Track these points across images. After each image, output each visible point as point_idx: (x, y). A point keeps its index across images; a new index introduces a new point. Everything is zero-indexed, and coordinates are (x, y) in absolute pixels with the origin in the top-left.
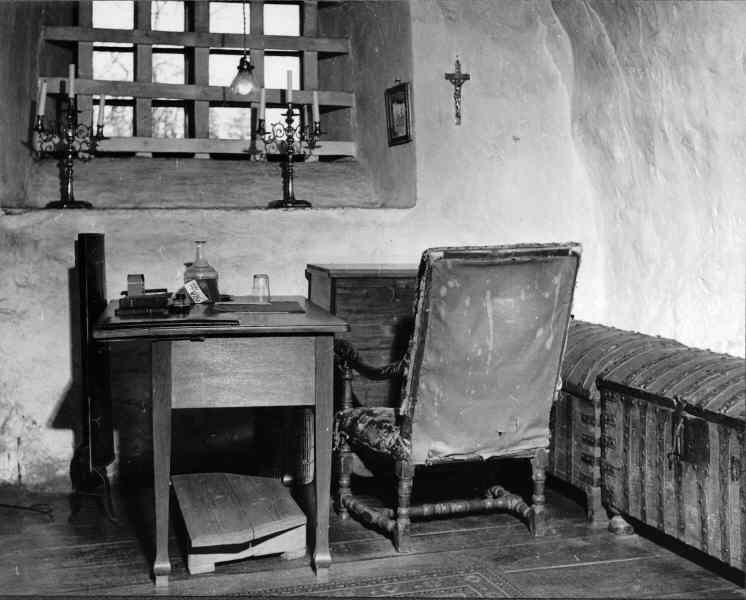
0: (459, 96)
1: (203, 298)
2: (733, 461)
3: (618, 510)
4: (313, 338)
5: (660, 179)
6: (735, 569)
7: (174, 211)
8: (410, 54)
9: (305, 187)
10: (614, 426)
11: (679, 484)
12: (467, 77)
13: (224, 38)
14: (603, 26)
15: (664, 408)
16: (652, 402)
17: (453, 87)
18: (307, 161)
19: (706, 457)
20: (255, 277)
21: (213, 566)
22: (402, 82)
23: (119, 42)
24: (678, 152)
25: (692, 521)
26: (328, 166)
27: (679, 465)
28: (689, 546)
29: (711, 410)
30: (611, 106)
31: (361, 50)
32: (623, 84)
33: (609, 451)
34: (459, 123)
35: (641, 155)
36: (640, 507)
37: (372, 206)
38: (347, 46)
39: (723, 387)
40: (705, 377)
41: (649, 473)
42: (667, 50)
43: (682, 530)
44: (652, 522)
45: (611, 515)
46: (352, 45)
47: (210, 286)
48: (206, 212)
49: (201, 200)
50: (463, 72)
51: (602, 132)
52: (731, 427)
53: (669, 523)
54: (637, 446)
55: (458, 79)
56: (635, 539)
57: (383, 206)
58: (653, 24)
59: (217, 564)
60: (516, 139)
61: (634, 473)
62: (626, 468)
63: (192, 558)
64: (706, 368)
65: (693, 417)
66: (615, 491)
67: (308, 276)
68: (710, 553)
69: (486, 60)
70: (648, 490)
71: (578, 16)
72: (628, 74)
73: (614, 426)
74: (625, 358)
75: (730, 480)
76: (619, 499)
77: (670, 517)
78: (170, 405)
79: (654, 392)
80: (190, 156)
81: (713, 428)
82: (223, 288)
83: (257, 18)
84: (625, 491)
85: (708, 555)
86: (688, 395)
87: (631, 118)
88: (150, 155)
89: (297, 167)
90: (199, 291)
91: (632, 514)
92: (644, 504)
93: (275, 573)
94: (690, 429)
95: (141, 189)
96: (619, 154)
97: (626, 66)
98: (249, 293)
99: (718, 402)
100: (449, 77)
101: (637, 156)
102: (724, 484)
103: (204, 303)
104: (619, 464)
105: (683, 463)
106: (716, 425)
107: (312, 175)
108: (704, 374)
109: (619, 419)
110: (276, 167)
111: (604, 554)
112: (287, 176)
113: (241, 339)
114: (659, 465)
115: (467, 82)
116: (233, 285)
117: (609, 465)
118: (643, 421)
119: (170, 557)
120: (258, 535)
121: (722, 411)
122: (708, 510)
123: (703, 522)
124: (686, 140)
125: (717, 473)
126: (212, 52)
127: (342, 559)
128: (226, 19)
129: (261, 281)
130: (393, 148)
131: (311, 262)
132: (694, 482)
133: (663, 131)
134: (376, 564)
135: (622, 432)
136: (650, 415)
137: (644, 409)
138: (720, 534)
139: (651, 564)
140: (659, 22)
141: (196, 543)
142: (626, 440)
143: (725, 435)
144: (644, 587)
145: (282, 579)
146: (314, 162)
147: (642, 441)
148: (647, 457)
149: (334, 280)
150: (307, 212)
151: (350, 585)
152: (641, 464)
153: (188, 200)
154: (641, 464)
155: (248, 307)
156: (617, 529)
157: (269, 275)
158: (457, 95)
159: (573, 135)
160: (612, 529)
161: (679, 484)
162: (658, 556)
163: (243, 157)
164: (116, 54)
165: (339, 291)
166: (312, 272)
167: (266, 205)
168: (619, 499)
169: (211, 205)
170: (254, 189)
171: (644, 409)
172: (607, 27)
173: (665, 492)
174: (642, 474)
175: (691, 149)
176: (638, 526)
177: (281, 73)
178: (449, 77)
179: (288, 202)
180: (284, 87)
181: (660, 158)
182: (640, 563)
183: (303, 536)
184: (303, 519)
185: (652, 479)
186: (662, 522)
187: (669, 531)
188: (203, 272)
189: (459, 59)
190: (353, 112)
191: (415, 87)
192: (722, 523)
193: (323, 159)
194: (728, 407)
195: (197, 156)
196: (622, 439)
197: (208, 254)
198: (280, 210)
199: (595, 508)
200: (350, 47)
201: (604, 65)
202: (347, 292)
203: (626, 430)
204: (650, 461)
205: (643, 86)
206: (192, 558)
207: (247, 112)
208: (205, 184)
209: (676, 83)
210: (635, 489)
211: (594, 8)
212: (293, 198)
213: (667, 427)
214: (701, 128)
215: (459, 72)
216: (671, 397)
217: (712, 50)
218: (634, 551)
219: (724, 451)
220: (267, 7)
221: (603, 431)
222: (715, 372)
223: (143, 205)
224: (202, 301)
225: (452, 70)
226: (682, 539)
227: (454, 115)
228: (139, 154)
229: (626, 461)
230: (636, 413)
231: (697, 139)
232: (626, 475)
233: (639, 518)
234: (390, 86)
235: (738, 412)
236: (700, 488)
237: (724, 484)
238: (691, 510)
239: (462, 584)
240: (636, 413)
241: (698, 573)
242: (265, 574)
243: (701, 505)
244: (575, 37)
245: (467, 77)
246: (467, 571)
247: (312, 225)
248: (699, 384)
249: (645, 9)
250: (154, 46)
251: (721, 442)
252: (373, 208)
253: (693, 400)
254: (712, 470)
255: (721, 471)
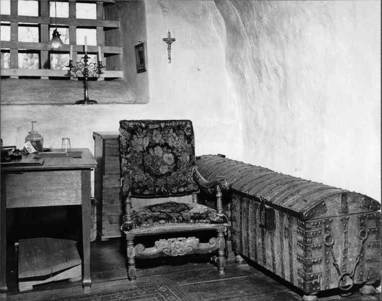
0: (170, 49)
1: (34, 150)
2: (285, 229)
3: (239, 252)
4: (80, 171)
5: (265, 89)
6: (287, 281)
7: (25, 106)
8: (145, 29)
9: (96, 93)
10: (236, 211)
11: (263, 240)
12: (174, 40)
13: (27, 18)
14: (238, 14)
15: (257, 202)
16: (252, 199)
17: (167, 44)
18: (98, 80)
19: (274, 227)
20: (63, 139)
21: (32, 287)
22: (142, 42)
23: (5, 21)
24: (273, 76)
25: (269, 257)
26: (109, 82)
27: (263, 231)
28: (268, 270)
29: (276, 204)
30: (243, 54)
31: (124, 26)
32: (249, 43)
33: (234, 223)
34: (170, 62)
35: (257, 78)
36: (247, 250)
37: (130, 103)
38: (118, 25)
39: (282, 192)
40: (275, 187)
41: (251, 234)
42: (267, 28)
43: (265, 263)
44: (252, 258)
45: (236, 255)
46: (121, 24)
47: (38, 145)
48: (42, 106)
49: (42, 100)
50: (172, 37)
51: (240, 66)
52: (284, 212)
53: (260, 259)
54: (245, 221)
55: (169, 41)
56: (246, 266)
57: (135, 103)
58: (260, 14)
59: (34, 286)
60: (198, 70)
61: (244, 234)
62: (241, 232)
63: (21, 284)
64: (277, 183)
65: (269, 207)
66: (237, 243)
67: (94, 138)
68: (277, 274)
69: (182, 30)
70: (250, 243)
71: (227, 10)
72: (250, 38)
73: (236, 211)
74: (242, 178)
75: (284, 238)
76: (238, 247)
77: (260, 256)
78: (6, 206)
79: (252, 194)
80: (39, 78)
81: (277, 212)
82: (45, 146)
83: (72, 10)
84: (241, 242)
85: (276, 275)
86: (266, 196)
87: (252, 58)
88: (18, 77)
89: (92, 83)
90: (32, 147)
91: (244, 254)
92: (249, 250)
93: (64, 289)
94: (267, 212)
95: (11, 95)
96: (247, 77)
97: (249, 34)
98: (60, 147)
99: (279, 200)
100: (164, 40)
101: (255, 78)
102: (282, 240)
103: (34, 153)
104: (238, 229)
105: (264, 229)
106: (278, 211)
107: (100, 87)
108: (275, 185)
109: (238, 208)
110: (81, 83)
111: (230, 275)
112: (85, 88)
113: (45, 172)
114: (255, 230)
115: (174, 42)
116: (51, 143)
117: (234, 230)
118: (248, 209)
119: (7, 283)
120: (54, 272)
121: (281, 205)
122: (276, 253)
123: (274, 258)
124: (276, 70)
125: (279, 234)
126: (78, 27)
127: (100, 281)
128: (60, 10)
129: (66, 141)
130: (139, 74)
131: (95, 131)
132: (269, 239)
133: (266, 66)
134: (114, 283)
135: (239, 214)
136: (250, 205)
137: (248, 202)
138: (281, 265)
139: (251, 279)
140: (263, 13)
141: (21, 276)
142: (241, 218)
143: (282, 216)
144: (245, 291)
145: (70, 291)
146: (102, 81)
147: (248, 219)
148: (250, 227)
149: (104, 140)
150: (94, 106)
151: (100, 295)
152: (247, 230)
153: (35, 100)
154: (247, 230)
155: (61, 155)
156: (239, 261)
157: (70, 138)
158: (169, 49)
159: (227, 68)
160: (236, 262)
161: (263, 240)
162: (255, 275)
163: (67, 78)
164: (30, 28)
165: (107, 146)
166: (96, 136)
167: (75, 102)
168: (238, 247)
169: (48, 102)
170: (70, 94)
171: (248, 202)
172: (240, 15)
173: (257, 244)
174: (248, 235)
175: (278, 75)
176: (247, 260)
177: (88, 38)
178: (164, 40)
179: (86, 101)
180: (83, 44)
181: (264, 79)
182: (247, 279)
183: (80, 270)
184: (81, 261)
185: (252, 237)
186: (256, 258)
187: (259, 263)
188: (36, 137)
189: (170, 31)
190: (121, 56)
191: (148, 45)
192: (281, 259)
193: (107, 79)
194: (283, 202)
195: (42, 78)
196: (239, 217)
197: (37, 128)
198: (80, 105)
199: (229, 251)
200: (120, 25)
201: (240, 34)
202: (111, 146)
203: (241, 213)
204: (251, 228)
205: (257, 44)
206: (21, 284)
207: (96, 56)
208: (45, 92)
209: (271, 43)
210: (245, 242)
211: (235, 6)
212: (88, 99)
213: (258, 211)
214: (284, 66)
215: (170, 37)
216: (259, 197)
217: (285, 26)
218: (245, 272)
219: (282, 224)
220: (78, 4)
221: (232, 213)
222: (281, 185)
223: (12, 103)
224: (33, 152)
225: (166, 36)
226: (265, 267)
227: (167, 58)
228: (11, 77)
229: (241, 228)
230: (245, 205)
231: (280, 71)
232: (241, 236)
233: (247, 256)
234: (137, 44)
235: (287, 205)
236: (272, 241)
237: (282, 240)
238: (269, 253)
239: (156, 292)
240: (245, 205)
241: (273, 283)
242: (60, 290)
243: (273, 251)
244: (227, 20)
245: (174, 40)
246: (161, 286)
247: (97, 112)
248: (273, 190)
249: (257, 7)
250: (2, 22)
251: (280, 219)
252: (130, 104)
253: (269, 199)
254: (277, 234)
255: (280, 233)
